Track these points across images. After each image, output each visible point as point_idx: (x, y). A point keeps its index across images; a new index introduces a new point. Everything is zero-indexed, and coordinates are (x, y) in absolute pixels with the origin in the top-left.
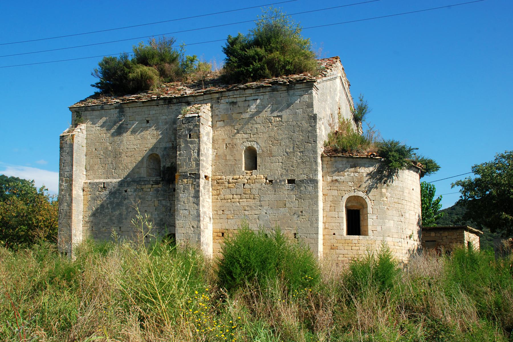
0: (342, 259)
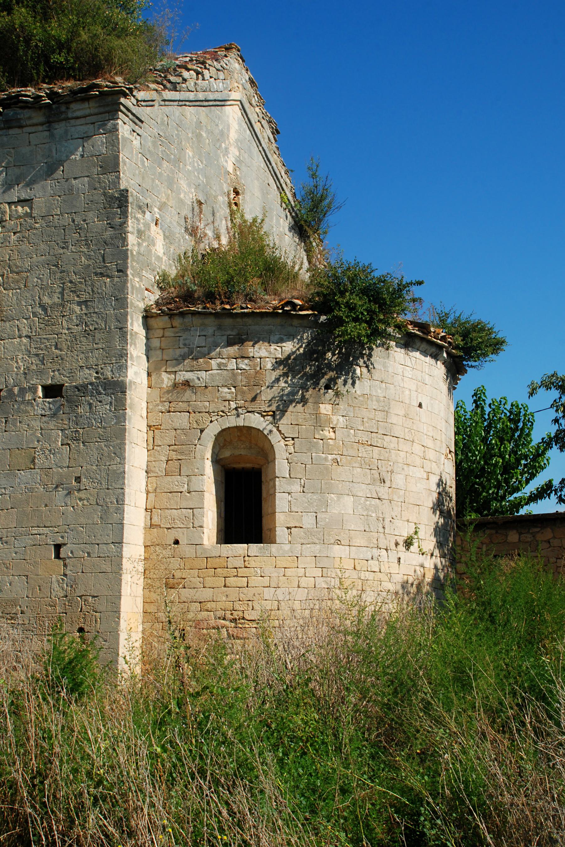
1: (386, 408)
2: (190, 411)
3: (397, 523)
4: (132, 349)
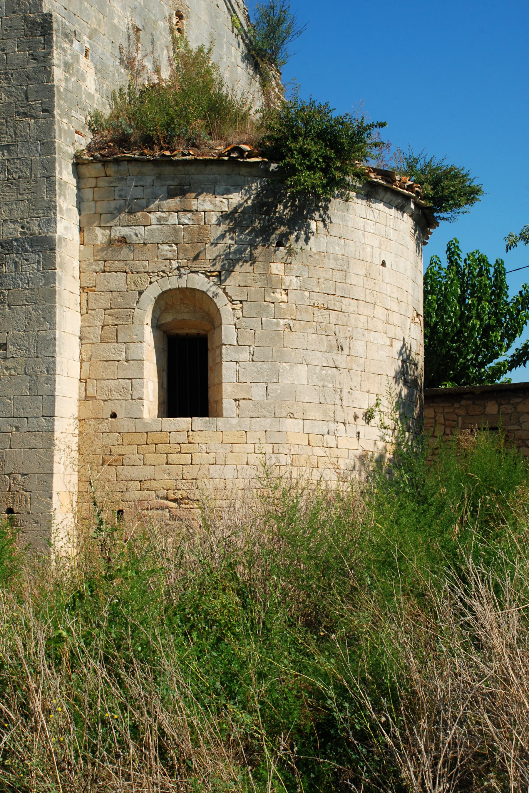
0: (138, 495)
1: (345, 267)
2: (128, 271)
3: (356, 394)
4: (61, 201)
